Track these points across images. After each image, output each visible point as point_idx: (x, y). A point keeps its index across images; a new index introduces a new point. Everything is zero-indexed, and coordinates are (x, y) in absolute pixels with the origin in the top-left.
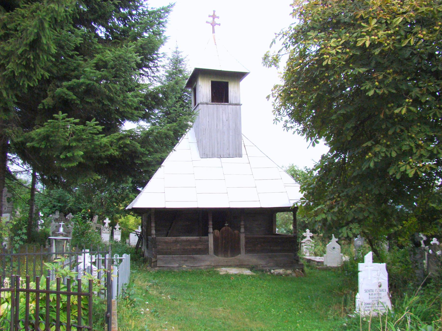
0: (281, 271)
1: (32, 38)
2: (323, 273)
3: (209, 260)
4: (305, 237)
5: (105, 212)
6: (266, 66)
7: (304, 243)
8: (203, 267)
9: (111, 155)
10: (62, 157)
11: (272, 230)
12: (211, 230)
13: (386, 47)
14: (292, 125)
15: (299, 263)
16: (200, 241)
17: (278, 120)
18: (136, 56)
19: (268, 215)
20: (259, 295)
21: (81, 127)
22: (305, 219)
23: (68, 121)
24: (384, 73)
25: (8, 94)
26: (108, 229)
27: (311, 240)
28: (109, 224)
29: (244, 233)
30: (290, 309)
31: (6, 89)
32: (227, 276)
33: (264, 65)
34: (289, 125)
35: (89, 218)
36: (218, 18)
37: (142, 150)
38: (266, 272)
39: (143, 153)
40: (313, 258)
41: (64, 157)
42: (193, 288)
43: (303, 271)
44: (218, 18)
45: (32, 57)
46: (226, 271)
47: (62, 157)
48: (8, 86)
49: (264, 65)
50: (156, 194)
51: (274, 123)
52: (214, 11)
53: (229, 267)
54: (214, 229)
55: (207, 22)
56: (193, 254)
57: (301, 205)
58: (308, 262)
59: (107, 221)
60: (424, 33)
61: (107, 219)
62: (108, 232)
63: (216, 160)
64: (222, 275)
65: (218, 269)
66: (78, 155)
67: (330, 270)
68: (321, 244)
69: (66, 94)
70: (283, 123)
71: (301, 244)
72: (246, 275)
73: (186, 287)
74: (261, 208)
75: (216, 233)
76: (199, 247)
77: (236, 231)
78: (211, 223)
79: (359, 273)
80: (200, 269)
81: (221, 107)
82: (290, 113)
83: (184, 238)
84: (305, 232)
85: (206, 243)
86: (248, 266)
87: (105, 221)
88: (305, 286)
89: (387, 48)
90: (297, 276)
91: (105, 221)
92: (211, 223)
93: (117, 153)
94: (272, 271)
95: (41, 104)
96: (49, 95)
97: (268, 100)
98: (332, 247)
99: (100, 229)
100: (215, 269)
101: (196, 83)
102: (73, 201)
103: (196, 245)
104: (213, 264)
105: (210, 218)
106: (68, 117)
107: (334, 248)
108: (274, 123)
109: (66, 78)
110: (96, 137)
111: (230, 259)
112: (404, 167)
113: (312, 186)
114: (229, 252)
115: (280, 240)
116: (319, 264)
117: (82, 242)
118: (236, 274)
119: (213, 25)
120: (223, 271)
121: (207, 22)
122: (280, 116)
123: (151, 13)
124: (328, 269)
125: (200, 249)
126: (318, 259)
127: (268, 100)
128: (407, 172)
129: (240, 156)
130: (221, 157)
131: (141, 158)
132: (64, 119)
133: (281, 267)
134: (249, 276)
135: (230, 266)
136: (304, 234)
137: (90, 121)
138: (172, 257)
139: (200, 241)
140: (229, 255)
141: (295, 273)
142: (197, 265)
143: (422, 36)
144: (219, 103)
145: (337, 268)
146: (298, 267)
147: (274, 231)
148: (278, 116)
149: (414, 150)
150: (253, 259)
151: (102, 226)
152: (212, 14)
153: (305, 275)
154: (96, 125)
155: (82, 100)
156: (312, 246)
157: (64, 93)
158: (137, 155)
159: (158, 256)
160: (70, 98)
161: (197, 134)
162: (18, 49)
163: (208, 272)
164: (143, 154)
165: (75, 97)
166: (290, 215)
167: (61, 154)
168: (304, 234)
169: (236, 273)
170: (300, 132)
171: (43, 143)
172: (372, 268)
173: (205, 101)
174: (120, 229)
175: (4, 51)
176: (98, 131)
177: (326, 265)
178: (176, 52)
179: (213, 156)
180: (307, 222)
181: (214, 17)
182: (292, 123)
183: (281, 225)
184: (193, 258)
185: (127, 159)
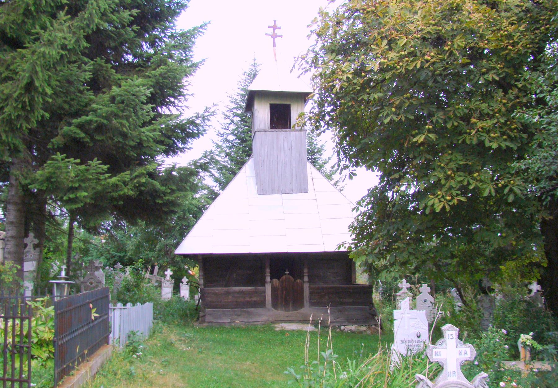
0: (353, 327)
1: (25, 82)
3: (267, 313)
4: (400, 289)
7: (400, 296)
8: (259, 323)
9: (124, 194)
10: (65, 198)
11: (351, 278)
12: (268, 279)
13: (398, 70)
18: (145, 89)
21: (83, 167)
23: (69, 162)
24: (402, 98)
25: (7, 136)
26: (169, 282)
28: (171, 276)
31: (5, 131)
32: (283, 332)
35: (142, 268)
36: (280, 28)
37: (163, 188)
41: (67, 198)
42: (235, 344)
44: (280, 28)
45: (27, 100)
46: (282, 327)
47: (65, 198)
48: (7, 129)
50: (205, 238)
52: (275, 21)
55: (267, 34)
56: (247, 308)
59: (169, 273)
60: (432, 54)
61: (169, 270)
62: (170, 286)
63: (277, 196)
64: (277, 331)
66: (80, 196)
69: (75, 133)
73: (226, 343)
74: (325, 252)
76: (255, 299)
77: (299, 281)
79: (395, 322)
80: (255, 325)
81: (282, 135)
83: (237, 289)
85: (263, 294)
87: (166, 273)
89: (398, 71)
90: (372, 333)
91: (166, 273)
92: (268, 270)
93: (131, 193)
95: (50, 144)
96: (60, 134)
99: (161, 281)
102: (132, 250)
103: (251, 297)
104: (271, 319)
106: (67, 157)
107: (425, 301)
109: (77, 114)
110: (102, 177)
111: (292, 313)
112: (432, 201)
114: (291, 304)
118: (293, 330)
119: (274, 36)
121: (267, 34)
123: (183, 35)
125: (255, 301)
128: (435, 207)
129: (306, 191)
131: (162, 197)
132: (63, 159)
133: (354, 323)
135: (291, 322)
137: (92, 161)
138: (223, 311)
139: (256, 292)
142: (252, 320)
143: (429, 58)
144: (280, 130)
149: (443, 182)
151: (163, 279)
152: (272, 24)
154: (100, 164)
155: (92, 138)
157: (71, 131)
160: (78, 136)
161: (256, 166)
162: (15, 92)
164: (165, 194)
165: (83, 135)
167: (65, 195)
171: (45, 185)
172: (409, 315)
173: (262, 127)
174: (187, 282)
175: (4, 94)
176: (103, 170)
178: (254, 65)
179: (273, 192)
181: (275, 27)
185: (148, 198)
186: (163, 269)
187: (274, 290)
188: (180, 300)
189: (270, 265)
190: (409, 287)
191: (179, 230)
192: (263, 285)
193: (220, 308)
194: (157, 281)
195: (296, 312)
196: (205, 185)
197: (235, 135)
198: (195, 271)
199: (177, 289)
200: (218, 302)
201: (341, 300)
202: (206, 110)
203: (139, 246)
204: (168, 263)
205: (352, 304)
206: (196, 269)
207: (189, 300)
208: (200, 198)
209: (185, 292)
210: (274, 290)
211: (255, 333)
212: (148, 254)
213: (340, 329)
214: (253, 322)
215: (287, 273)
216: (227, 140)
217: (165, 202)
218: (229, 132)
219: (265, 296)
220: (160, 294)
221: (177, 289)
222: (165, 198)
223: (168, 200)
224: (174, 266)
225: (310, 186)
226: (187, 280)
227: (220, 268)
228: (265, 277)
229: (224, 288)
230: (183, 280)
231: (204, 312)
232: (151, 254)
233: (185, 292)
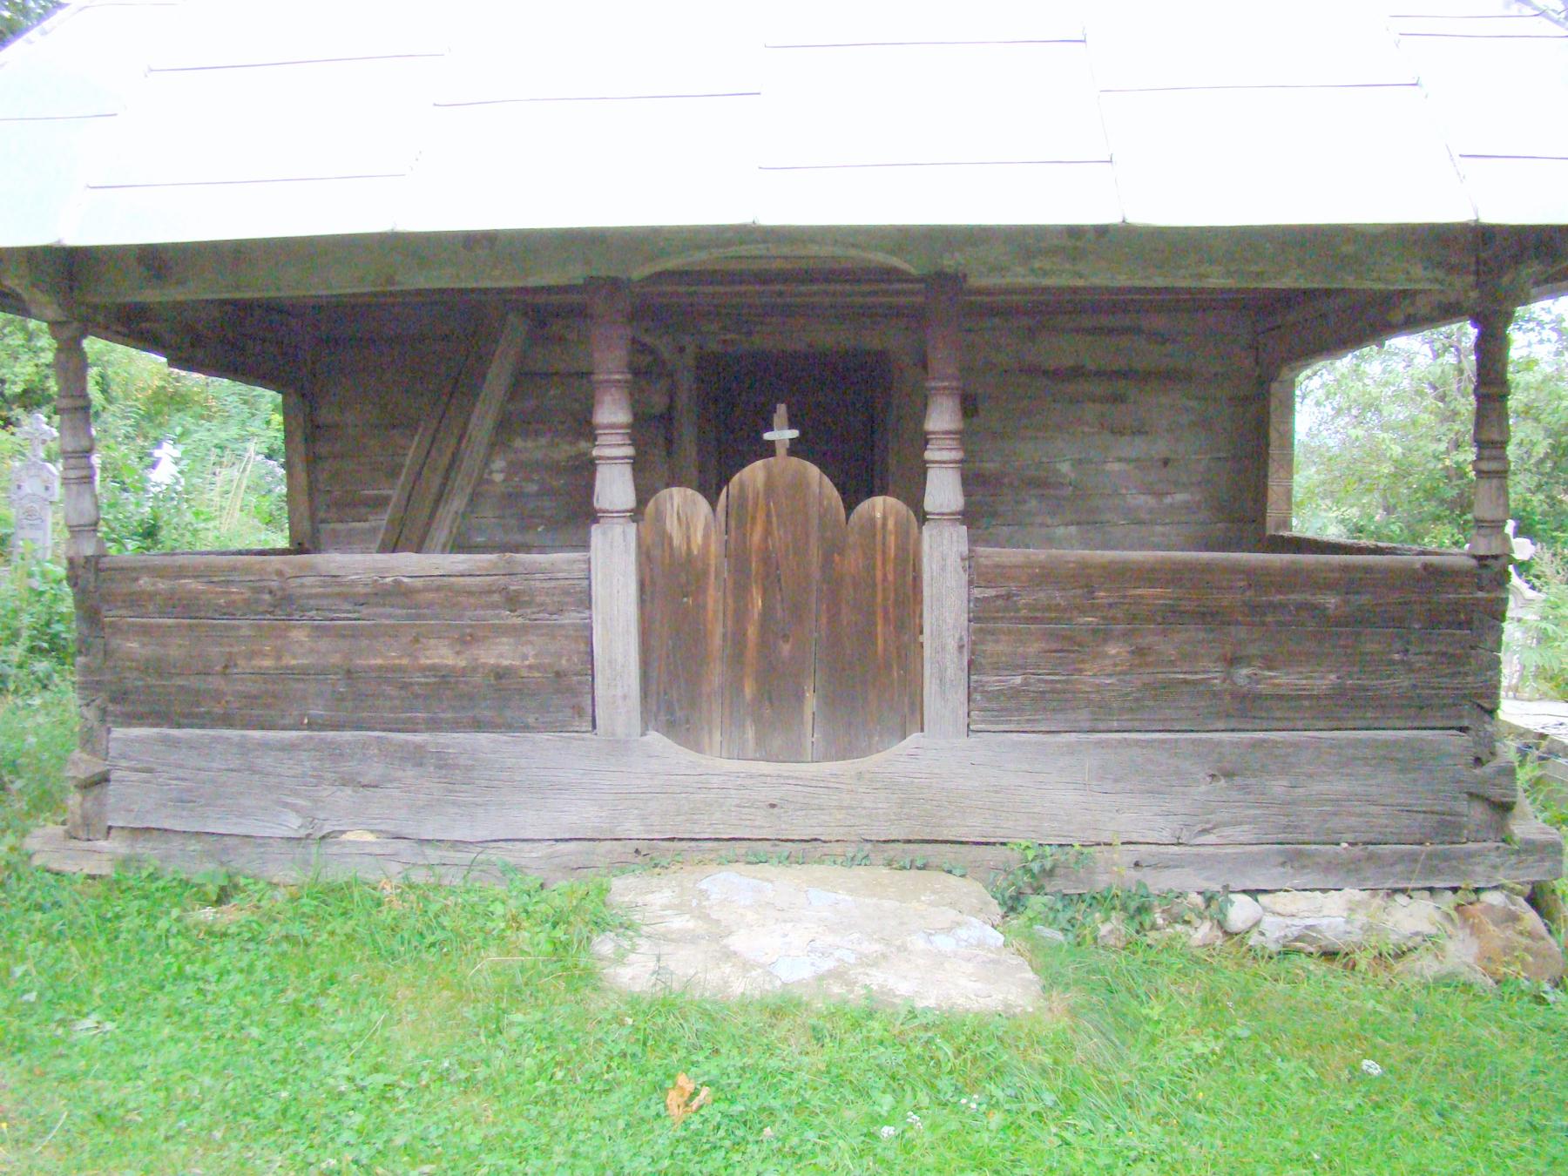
0: (1332, 912)
12: (614, 487)
56: (434, 725)
75: (672, 526)
76: (500, 653)
85: (571, 618)
92: (612, 413)
103: (467, 640)
104: (632, 827)
114: (811, 702)
115: (1331, 601)
117: (518, 1010)
138: (243, 748)
140: (812, 737)
141: (1476, 930)
159: (118, 732)
184: (444, 763)
193: (227, 721)
205: (1341, 707)
219: (585, 635)
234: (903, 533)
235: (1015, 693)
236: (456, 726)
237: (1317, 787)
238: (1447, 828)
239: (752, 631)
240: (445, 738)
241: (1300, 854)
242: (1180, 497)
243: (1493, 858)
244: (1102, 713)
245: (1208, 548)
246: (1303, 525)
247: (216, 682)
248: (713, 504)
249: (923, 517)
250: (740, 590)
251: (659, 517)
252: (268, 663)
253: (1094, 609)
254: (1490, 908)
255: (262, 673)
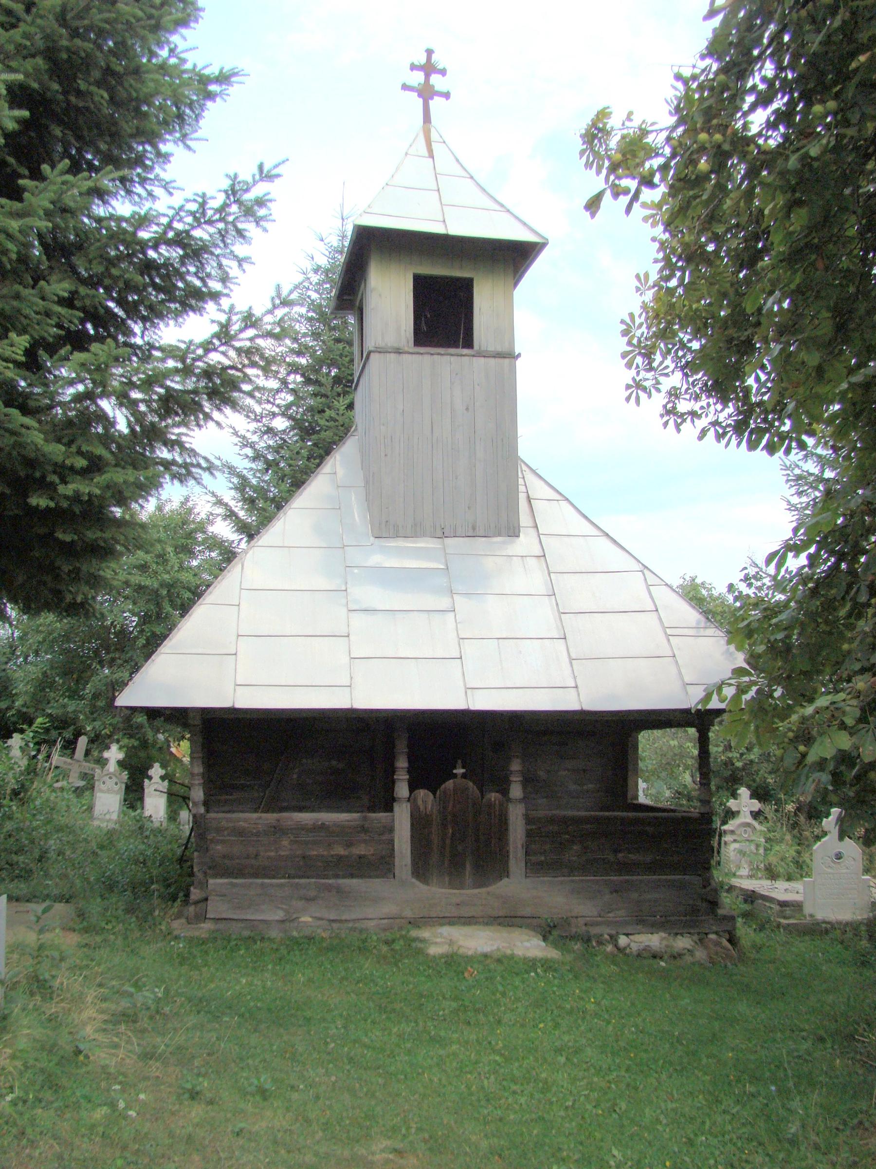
0: (654, 940)
2: (802, 946)
3: (393, 897)
4: (731, 814)
5: (121, 726)
6: (598, 173)
7: (732, 832)
8: (372, 923)
14: (696, 406)
15: (721, 912)
16: (363, 829)
17: (644, 389)
19: (605, 738)
20: (562, 1060)
22: (735, 755)
26: (115, 780)
27: (755, 824)
28: (120, 763)
29: (520, 801)
30: (691, 1143)
32: (454, 962)
33: (588, 165)
34: (683, 406)
36: (443, 72)
38: (600, 943)
39: (63, 466)
40: (761, 886)
43: (732, 940)
44: (443, 72)
46: (451, 943)
49: (588, 165)
51: (628, 399)
52: (430, 52)
53: (465, 924)
54: (413, 786)
55: (405, 87)
56: (337, 876)
57: (736, 698)
58: (746, 901)
59: (114, 754)
61: (114, 747)
62: (116, 788)
65: (425, 933)
67: (827, 932)
68: (788, 837)
70: (659, 400)
71: (720, 836)
72: (526, 960)
75: (420, 802)
76: (360, 850)
78: (402, 763)
81: (444, 363)
82: (687, 363)
84: (734, 795)
85: (386, 837)
86: (535, 922)
87: (106, 754)
88: (743, 1007)
92: (402, 763)
94: (623, 941)
97: (593, 215)
98: (832, 854)
100: (414, 933)
101: (363, 286)
103: (349, 844)
104: (408, 913)
105: (402, 746)
108: (628, 399)
113: (782, 616)
116: (788, 911)
118: (486, 956)
119: (426, 93)
120: (440, 940)
121: (405, 87)
122: (650, 375)
124: (818, 930)
126: (780, 890)
127: (593, 215)
130: (444, 536)
131: (52, 486)
133: (654, 927)
134: (532, 964)
135: (469, 921)
136: (732, 804)
139: (363, 829)
141: (707, 948)
142: (353, 917)
145: (853, 927)
146: (714, 928)
147: (630, 794)
148: (643, 374)
150: (554, 896)
152: (423, 60)
153: (742, 958)
156: (758, 846)
158: (38, 474)
163: (387, 942)
164: (64, 472)
166: (685, 741)
168: (732, 804)
169: (487, 949)
170: (724, 434)
173: (391, 340)
177: (811, 916)
179: (416, 531)
180: (739, 764)
181: (429, 68)
182: (697, 398)
183: (654, 772)
184: (339, 890)
186: (99, 741)
187: (420, 823)
188: (141, 827)
189: (409, 746)
190: (756, 809)
191: (144, 646)
192: (389, 808)
193: (256, 875)
194: (84, 776)
195: (483, 890)
196: (214, 537)
197: (290, 418)
198: (182, 749)
199: (134, 793)
200: (248, 857)
201: (620, 855)
202: (234, 192)
203: (44, 684)
204: (115, 729)
205: (651, 868)
206: (185, 745)
207: (165, 824)
208: (198, 567)
209: (155, 804)
210: (419, 823)
211: (368, 966)
212: (64, 706)
213: (616, 946)
214: (354, 920)
215: (459, 771)
216: (270, 431)
217: (65, 504)
218: (276, 410)
219: (391, 842)
220: (91, 808)
221: (134, 793)
222: (62, 489)
223: (76, 498)
224: (131, 736)
225: (524, 519)
226: (162, 772)
227: (252, 751)
228: (393, 782)
229: (264, 815)
230: (151, 772)
231: (203, 885)
232: (72, 706)
233: (155, 804)
234: (501, 805)
235: (541, 864)
236: (344, 877)
237: (649, 896)
238: (695, 911)
239: (448, 841)
240: (341, 881)
241: (645, 920)
242: (591, 786)
243: (711, 922)
244: (572, 870)
245: (601, 810)
246: (642, 799)
247: (253, 862)
248: (434, 794)
249: (509, 800)
250: (444, 826)
251: (415, 800)
252: (272, 854)
253: (568, 833)
254: (711, 940)
255: (269, 857)
